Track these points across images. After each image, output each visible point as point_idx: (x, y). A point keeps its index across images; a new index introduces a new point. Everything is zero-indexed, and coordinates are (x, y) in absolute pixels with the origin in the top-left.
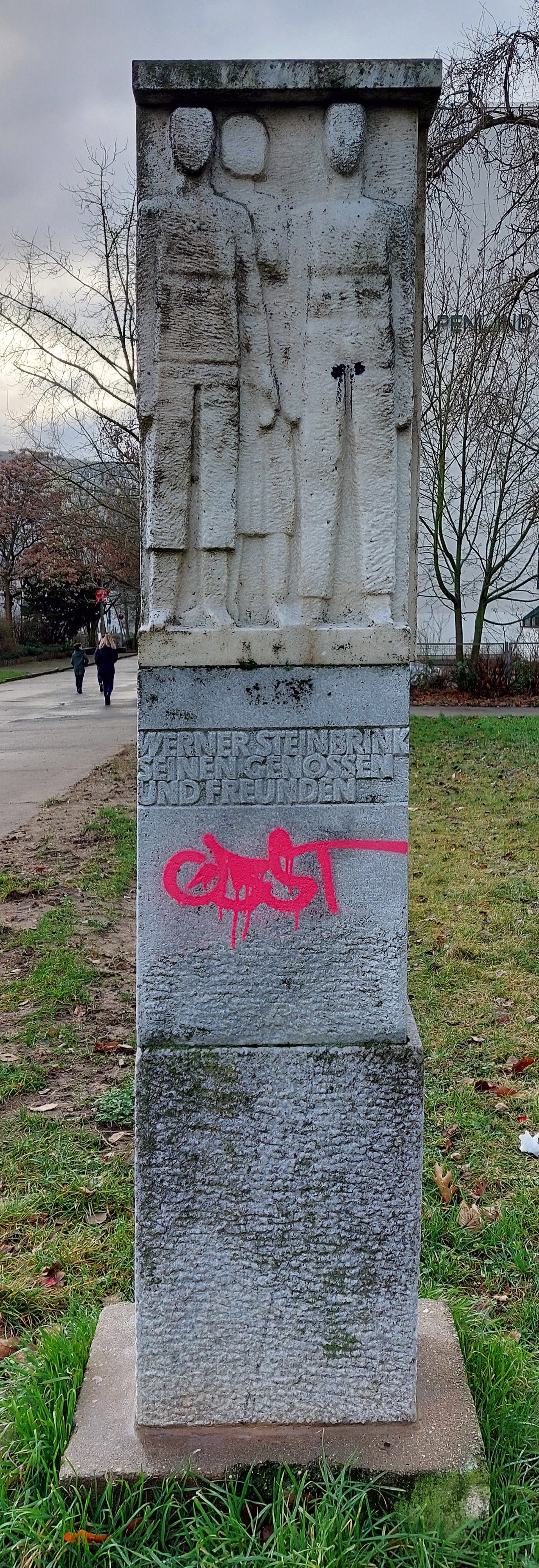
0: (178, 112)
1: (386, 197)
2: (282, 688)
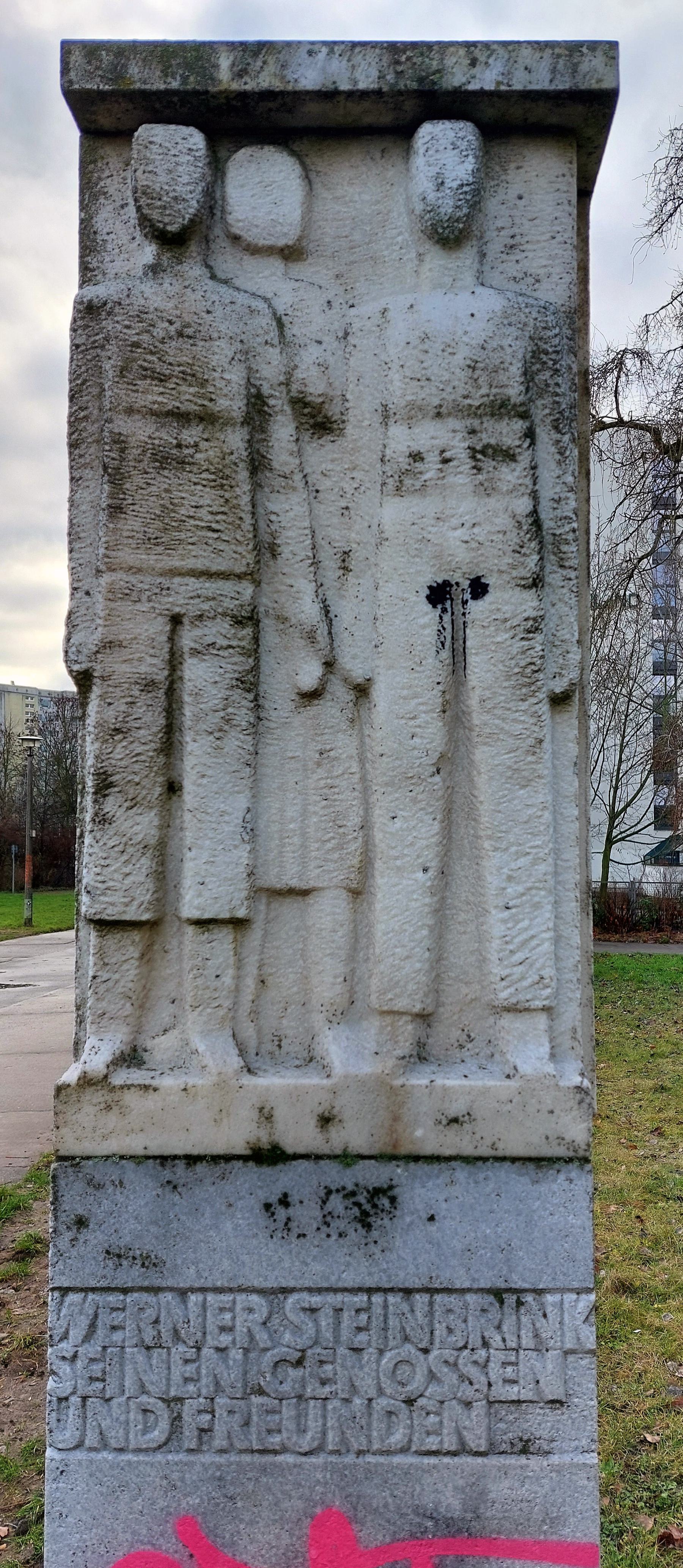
0: (144, 131)
1: (522, 287)
2: (336, 1203)
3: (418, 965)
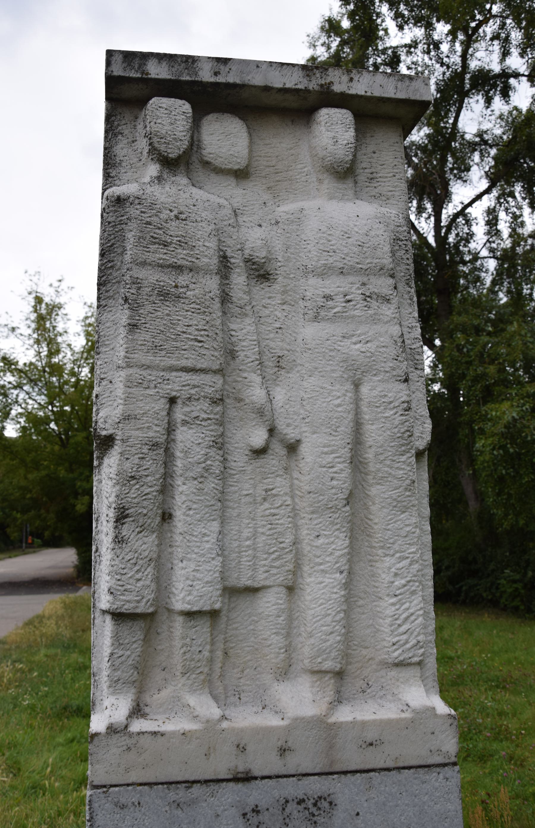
2: (292, 807)
3: (338, 638)
